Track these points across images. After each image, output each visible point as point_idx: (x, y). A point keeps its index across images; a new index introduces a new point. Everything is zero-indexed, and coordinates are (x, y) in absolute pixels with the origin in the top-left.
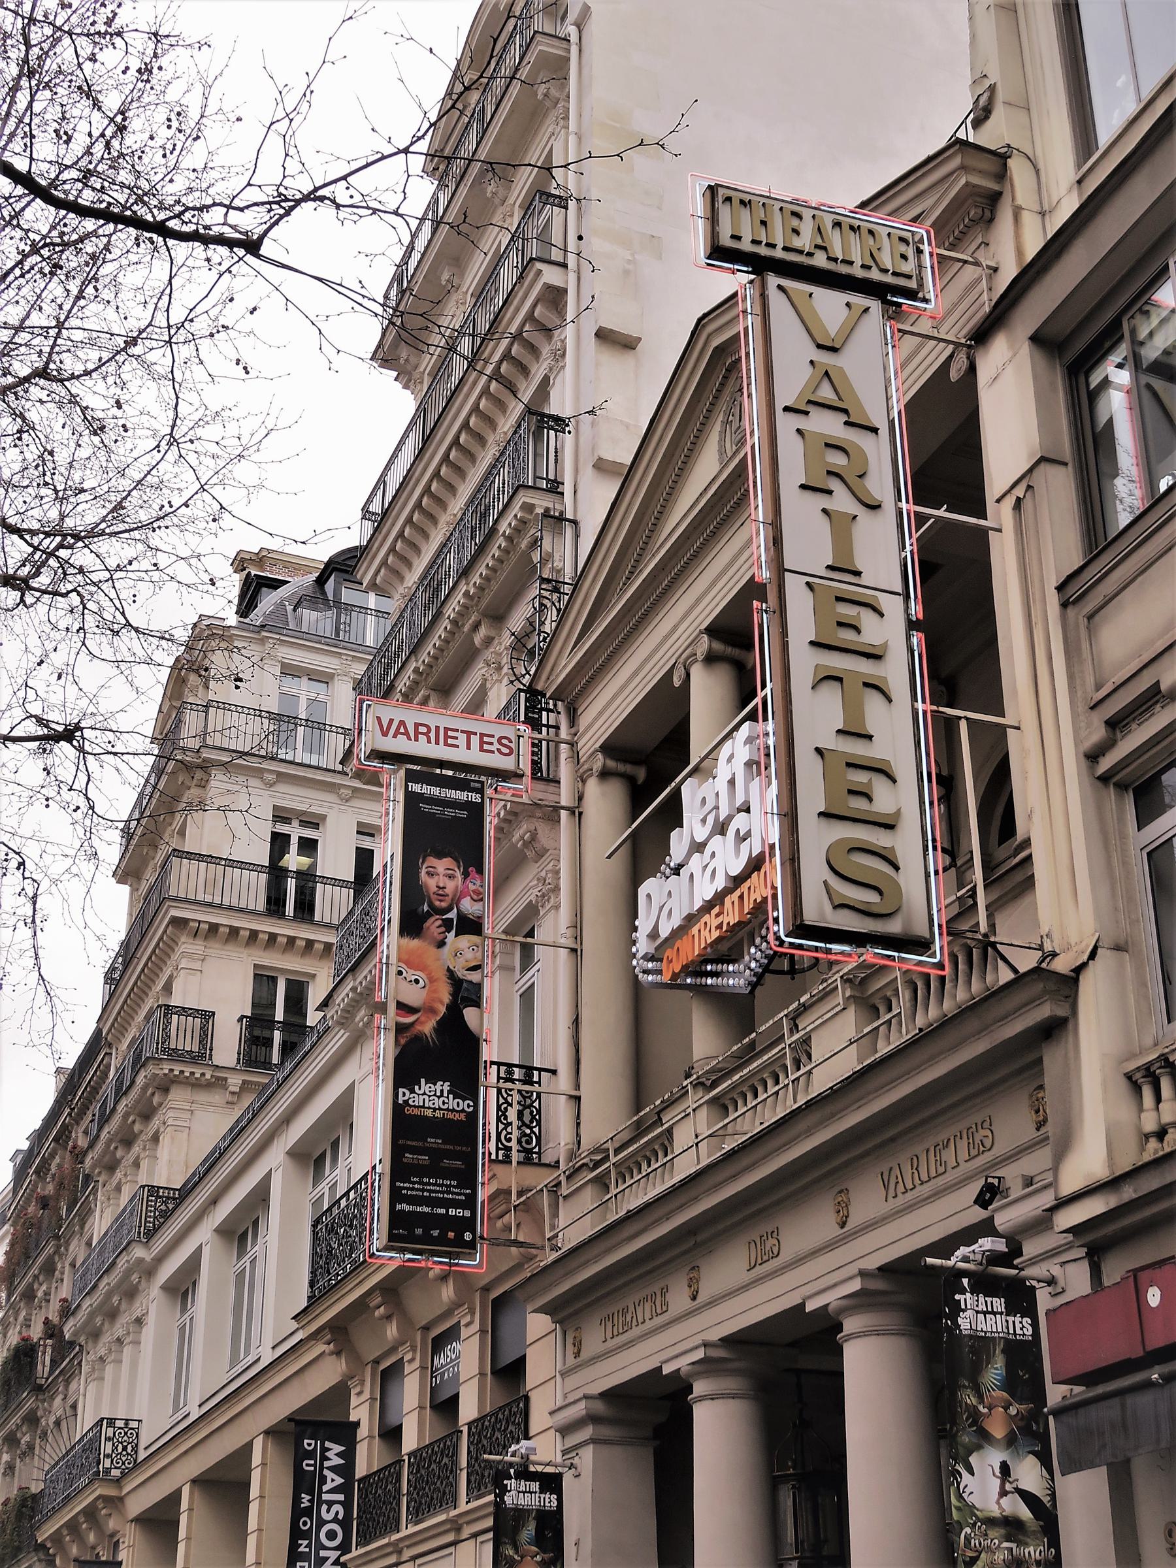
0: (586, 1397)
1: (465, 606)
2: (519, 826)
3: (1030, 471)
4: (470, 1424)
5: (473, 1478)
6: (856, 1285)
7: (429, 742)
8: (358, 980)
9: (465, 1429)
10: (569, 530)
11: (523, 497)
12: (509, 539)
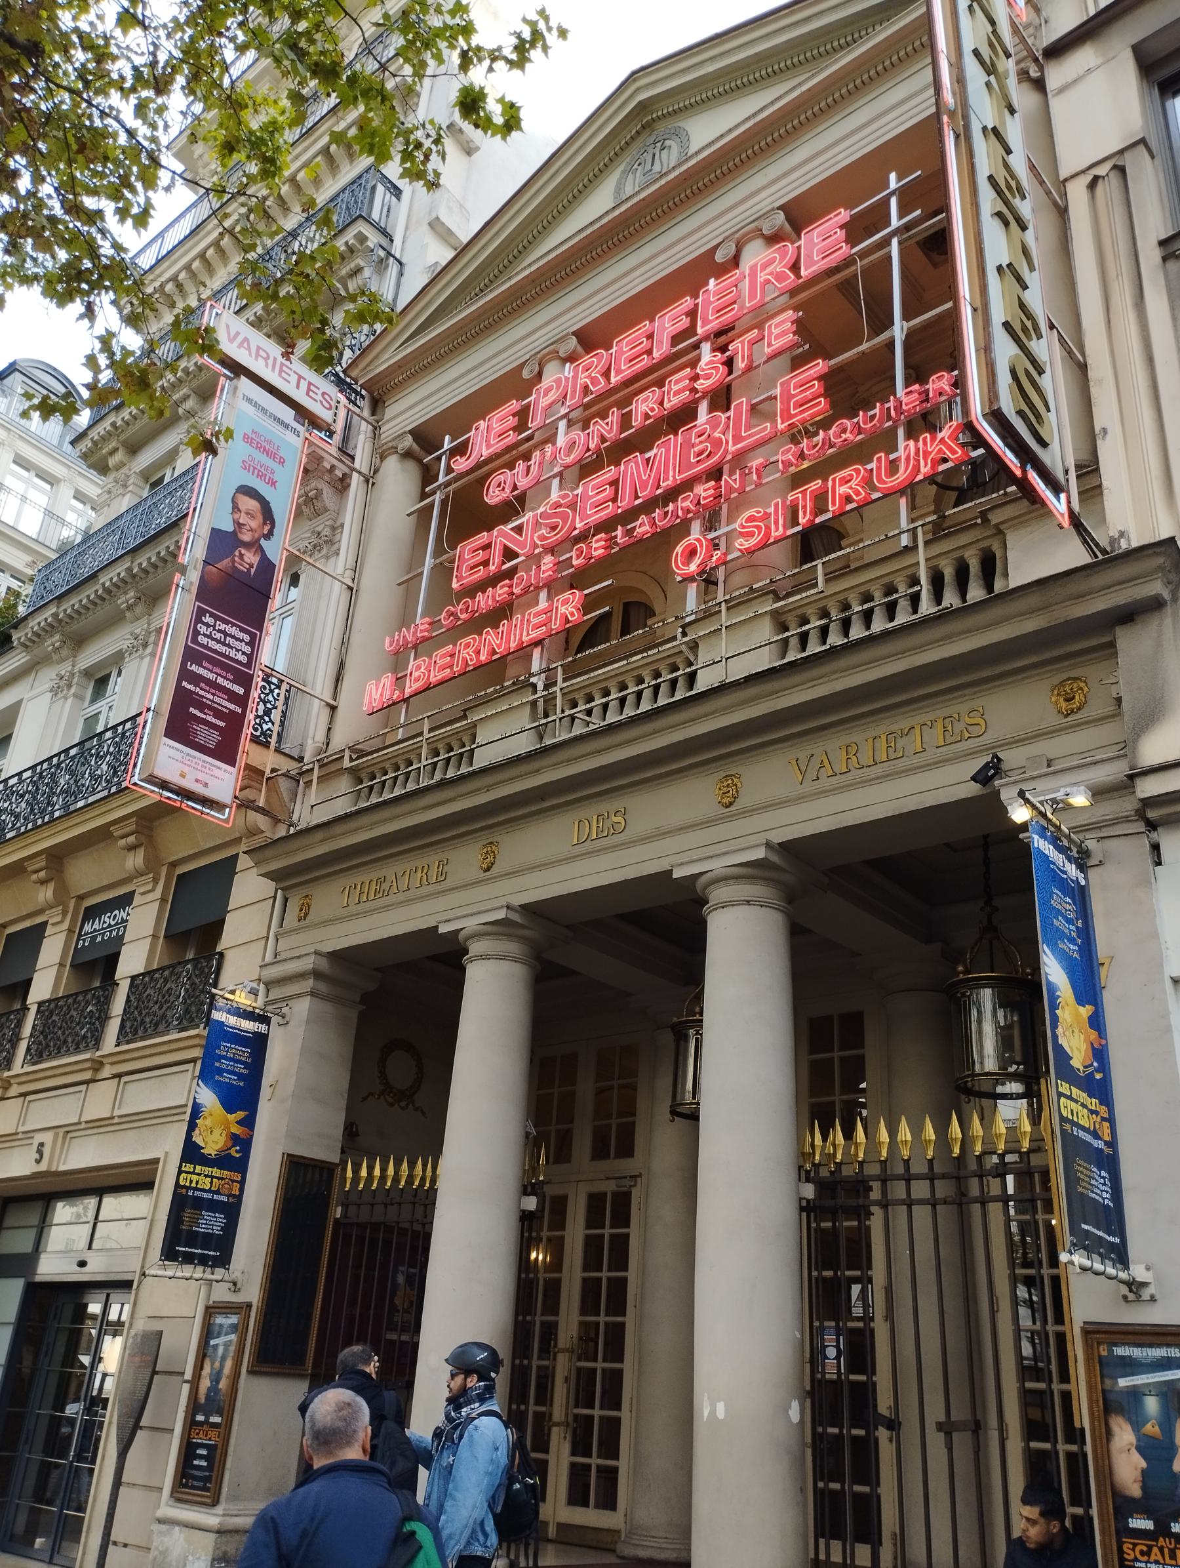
0: (316, 953)
1: (109, 433)
2: (126, 593)
3: (1121, 152)
4: (40, 1004)
5: (128, 1024)
6: (501, 915)
7: (267, 365)
8: (62, 608)
9: (33, 1009)
10: (393, 268)
11: (361, 227)
12: (95, 443)
